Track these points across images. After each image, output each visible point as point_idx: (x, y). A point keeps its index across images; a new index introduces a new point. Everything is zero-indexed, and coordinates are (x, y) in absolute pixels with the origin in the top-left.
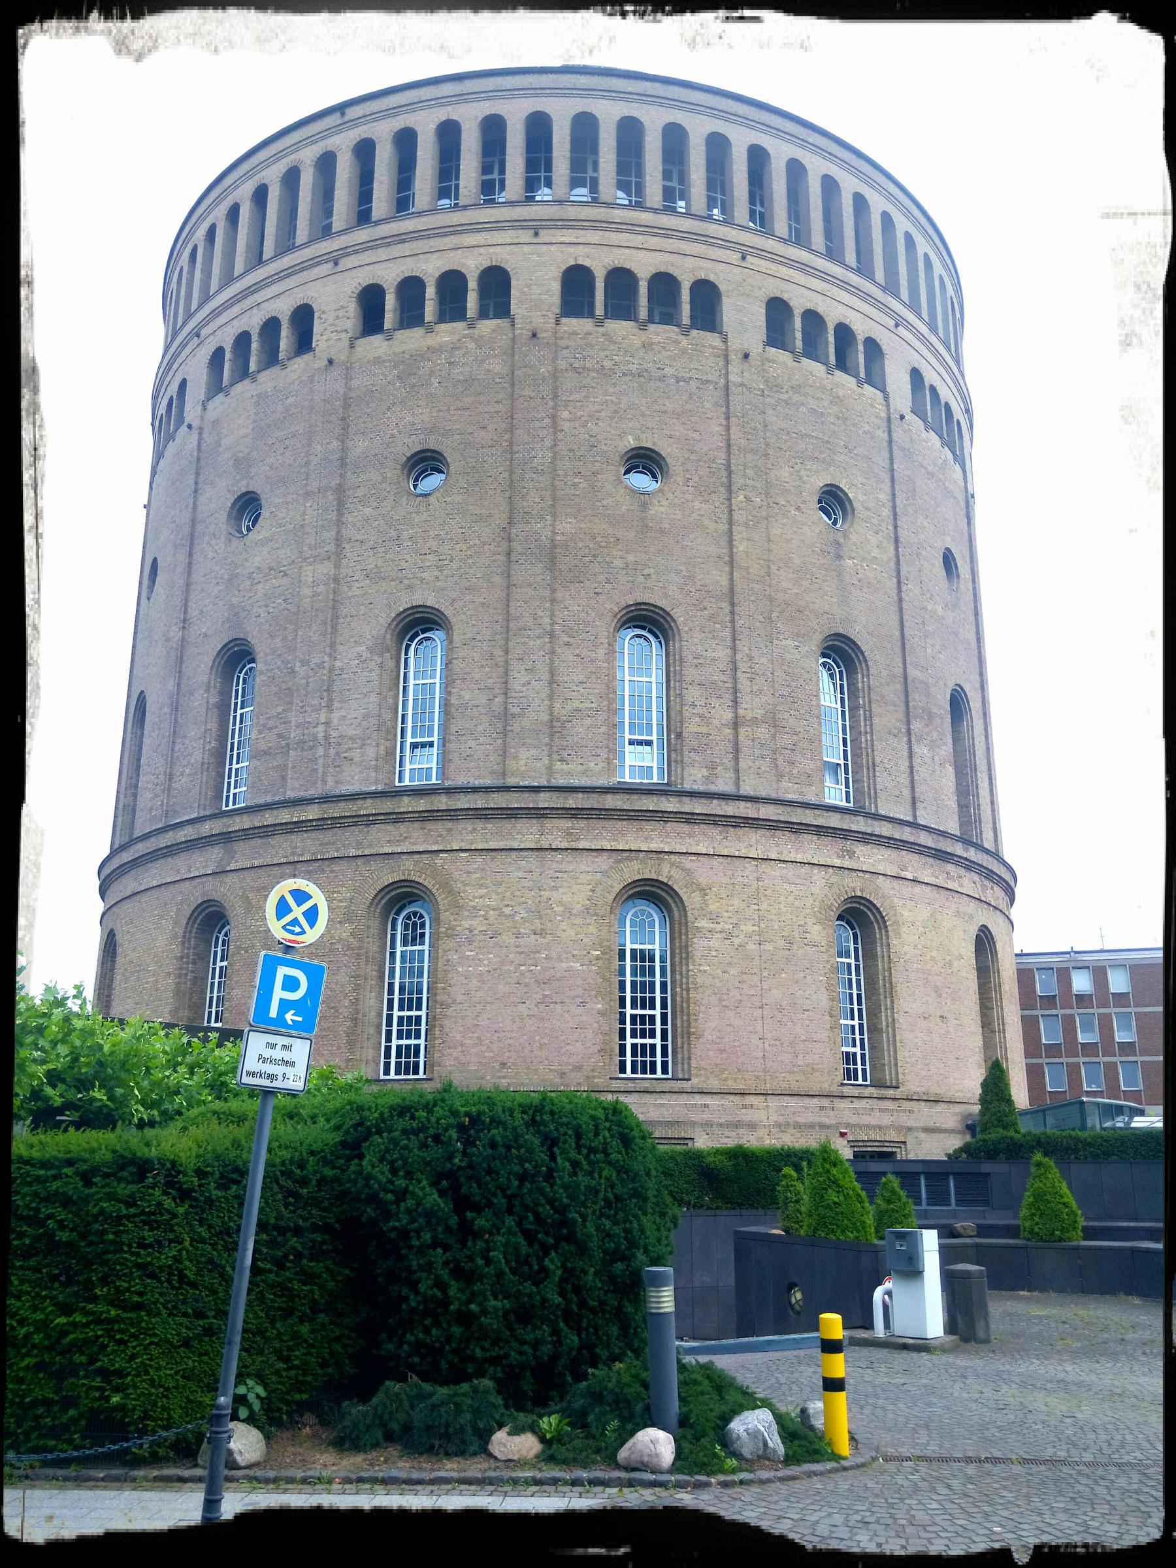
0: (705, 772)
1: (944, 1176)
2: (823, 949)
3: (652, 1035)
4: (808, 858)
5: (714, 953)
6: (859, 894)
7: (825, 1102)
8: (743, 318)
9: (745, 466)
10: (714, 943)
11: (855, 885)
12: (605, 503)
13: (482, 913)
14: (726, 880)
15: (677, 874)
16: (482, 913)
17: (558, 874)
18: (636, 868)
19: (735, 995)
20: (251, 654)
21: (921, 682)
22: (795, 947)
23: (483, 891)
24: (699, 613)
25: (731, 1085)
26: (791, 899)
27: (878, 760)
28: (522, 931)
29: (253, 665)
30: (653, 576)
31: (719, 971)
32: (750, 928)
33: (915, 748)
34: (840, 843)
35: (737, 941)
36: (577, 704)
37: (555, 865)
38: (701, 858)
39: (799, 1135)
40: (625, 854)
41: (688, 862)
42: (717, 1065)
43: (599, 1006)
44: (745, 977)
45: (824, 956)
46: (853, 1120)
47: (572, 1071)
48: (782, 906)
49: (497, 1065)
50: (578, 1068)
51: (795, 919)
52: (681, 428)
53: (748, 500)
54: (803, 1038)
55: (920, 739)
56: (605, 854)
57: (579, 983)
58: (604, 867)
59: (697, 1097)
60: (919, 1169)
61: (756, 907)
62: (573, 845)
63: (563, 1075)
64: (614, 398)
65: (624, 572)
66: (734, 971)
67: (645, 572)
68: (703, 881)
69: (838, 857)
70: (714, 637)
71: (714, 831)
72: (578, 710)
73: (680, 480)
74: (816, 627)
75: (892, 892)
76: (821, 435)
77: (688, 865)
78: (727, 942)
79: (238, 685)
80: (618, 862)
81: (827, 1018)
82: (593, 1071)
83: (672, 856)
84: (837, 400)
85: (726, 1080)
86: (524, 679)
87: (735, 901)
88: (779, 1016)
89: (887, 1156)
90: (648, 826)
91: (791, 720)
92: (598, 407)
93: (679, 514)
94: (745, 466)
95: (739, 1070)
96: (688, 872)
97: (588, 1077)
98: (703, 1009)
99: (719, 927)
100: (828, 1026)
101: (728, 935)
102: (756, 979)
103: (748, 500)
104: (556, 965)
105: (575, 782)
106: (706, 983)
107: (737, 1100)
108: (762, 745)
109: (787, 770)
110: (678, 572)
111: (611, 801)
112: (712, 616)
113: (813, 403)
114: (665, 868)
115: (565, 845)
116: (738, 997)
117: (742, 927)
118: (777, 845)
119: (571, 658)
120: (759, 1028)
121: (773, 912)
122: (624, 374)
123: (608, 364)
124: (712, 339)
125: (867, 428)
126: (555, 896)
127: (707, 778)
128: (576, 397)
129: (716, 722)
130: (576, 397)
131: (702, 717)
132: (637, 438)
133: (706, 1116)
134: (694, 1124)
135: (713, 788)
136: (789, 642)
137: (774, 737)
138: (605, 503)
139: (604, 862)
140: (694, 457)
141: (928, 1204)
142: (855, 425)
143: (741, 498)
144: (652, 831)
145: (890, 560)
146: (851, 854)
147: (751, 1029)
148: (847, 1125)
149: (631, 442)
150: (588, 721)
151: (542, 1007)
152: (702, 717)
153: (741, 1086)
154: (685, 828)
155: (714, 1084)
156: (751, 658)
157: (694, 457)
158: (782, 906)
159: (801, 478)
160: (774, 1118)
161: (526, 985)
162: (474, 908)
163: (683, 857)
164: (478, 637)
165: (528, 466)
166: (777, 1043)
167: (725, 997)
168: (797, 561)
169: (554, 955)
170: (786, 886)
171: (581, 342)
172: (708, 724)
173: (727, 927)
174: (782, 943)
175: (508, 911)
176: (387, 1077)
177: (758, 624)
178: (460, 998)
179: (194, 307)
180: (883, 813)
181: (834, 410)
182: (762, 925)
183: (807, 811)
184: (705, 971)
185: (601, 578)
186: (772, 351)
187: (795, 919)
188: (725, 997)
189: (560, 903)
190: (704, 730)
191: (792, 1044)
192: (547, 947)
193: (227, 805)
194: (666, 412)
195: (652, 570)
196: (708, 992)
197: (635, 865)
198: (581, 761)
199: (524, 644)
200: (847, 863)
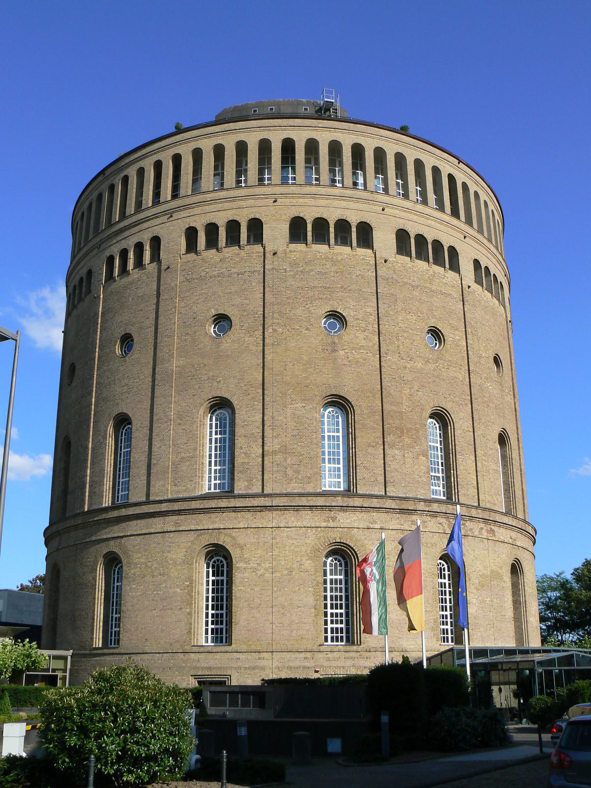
0: (246, 483)
1: (237, 693)
2: (312, 573)
3: (222, 624)
4: (305, 524)
5: (246, 580)
6: (338, 540)
7: (308, 655)
8: (276, 233)
9: (273, 313)
10: (246, 574)
11: (336, 536)
12: (199, 347)
13: (139, 566)
14: (255, 540)
15: (228, 539)
16: (139, 566)
17: (171, 544)
18: (207, 538)
19: (257, 601)
20: (128, 420)
21: (396, 412)
22: (294, 573)
23: (140, 555)
24: (246, 397)
25: (253, 648)
26: (293, 547)
27: (358, 462)
28: (155, 574)
29: (130, 426)
30: (222, 382)
31: (249, 589)
32: (267, 565)
33: (388, 451)
34: (327, 513)
35: (259, 573)
36: (183, 455)
37: (170, 540)
38: (241, 530)
39: (290, 672)
40: (202, 531)
41: (234, 533)
42: (246, 638)
43: (188, 610)
44: (263, 592)
45: (313, 577)
46: (326, 664)
47: (175, 642)
48: (287, 552)
49: (144, 640)
50: (177, 641)
51: (294, 558)
52: (239, 299)
53: (274, 330)
54: (297, 621)
55: (392, 446)
56: (193, 532)
57: (179, 599)
58: (192, 539)
59: (235, 654)
60: (238, 690)
61: (271, 554)
62: (178, 529)
63: (171, 644)
64: (205, 291)
65: (207, 381)
66: (257, 589)
67: (218, 380)
68: (241, 542)
69: (325, 521)
70: (253, 409)
71: (248, 515)
72: (183, 458)
73: (238, 327)
74: (317, 393)
75: (363, 538)
76: (324, 285)
77: (234, 535)
78: (254, 573)
79: (122, 436)
80: (198, 536)
81: (313, 610)
82: (184, 642)
83: (225, 530)
84: (334, 262)
85: (250, 645)
86: (159, 445)
87: (259, 552)
88: (282, 611)
89: (222, 683)
90: (213, 515)
91: (298, 448)
92: (197, 297)
93: (236, 346)
94: (273, 313)
95: (258, 640)
96: (234, 538)
97: (182, 645)
98: (239, 610)
99: (249, 566)
100: (313, 615)
101: (255, 570)
102: (270, 592)
103: (274, 330)
104: (169, 590)
105: (181, 496)
106: (242, 596)
107: (256, 655)
108: (278, 465)
109: (295, 476)
110: (235, 377)
111: (194, 505)
112: (253, 398)
113: (319, 269)
114: (222, 537)
115: (174, 529)
116: (260, 602)
117: (263, 565)
118: (285, 518)
119: (181, 431)
120: (270, 618)
121: (281, 555)
122: (211, 277)
123: (203, 274)
124: (258, 248)
125: (358, 273)
126: (170, 555)
127: (247, 486)
128: (188, 294)
129: (253, 455)
130: (188, 294)
131: (245, 454)
132: (217, 310)
133: (239, 664)
134: (231, 668)
135: (250, 492)
136: (300, 405)
137: (286, 460)
138: (199, 347)
139: (192, 536)
140: (245, 313)
141: (242, 707)
142: (350, 273)
143: (271, 330)
144: (216, 518)
145: (374, 345)
146: (334, 519)
147: (266, 618)
148: (322, 666)
149: (214, 312)
150: (188, 463)
151: (163, 611)
152: (245, 454)
153: (259, 648)
154: (233, 514)
155: (244, 647)
156: (273, 418)
157: (245, 313)
158: (287, 552)
159: (309, 312)
160: (276, 664)
161: (156, 601)
162: (136, 563)
163: (232, 530)
164: (142, 426)
165: (164, 335)
166: (281, 625)
167: (252, 603)
168: (305, 358)
169: (168, 586)
170: (290, 541)
171: (191, 266)
172: (249, 457)
173: (254, 565)
174: (286, 572)
175: (149, 564)
176: (207, 644)
177: (278, 398)
178: (130, 608)
179: (76, 253)
180: (361, 492)
181: (334, 269)
182: (274, 563)
183: (303, 498)
184: (241, 590)
185: (196, 386)
186: (293, 246)
187: (294, 558)
188: (252, 603)
189: (171, 559)
190: (246, 460)
191: (289, 625)
192: (165, 581)
193: (118, 501)
194: (231, 293)
195: (221, 378)
196: (242, 601)
197: (207, 536)
198: (183, 484)
199: (159, 427)
200: (331, 524)
